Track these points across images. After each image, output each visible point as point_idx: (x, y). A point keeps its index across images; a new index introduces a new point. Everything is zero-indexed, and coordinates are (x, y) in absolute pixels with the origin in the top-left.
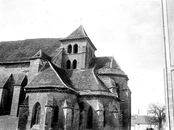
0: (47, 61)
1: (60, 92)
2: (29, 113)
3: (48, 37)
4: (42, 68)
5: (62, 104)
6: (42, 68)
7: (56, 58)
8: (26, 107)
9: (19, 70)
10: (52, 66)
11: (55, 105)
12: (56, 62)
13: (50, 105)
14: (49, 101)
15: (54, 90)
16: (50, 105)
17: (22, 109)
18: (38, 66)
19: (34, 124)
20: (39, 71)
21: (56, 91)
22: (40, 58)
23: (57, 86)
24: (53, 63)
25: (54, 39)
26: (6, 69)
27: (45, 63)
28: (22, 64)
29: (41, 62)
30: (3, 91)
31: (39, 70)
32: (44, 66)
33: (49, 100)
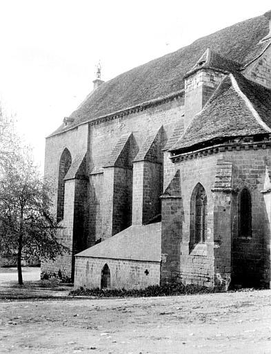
0: (225, 74)
1: (251, 147)
2: (183, 213)
3: (241, 20)
4: (213, 95)
5: (258, 183)
6: (213, 95)
7: (258, 61)
8: (175, 198)
9: (176, 113)
10: (237, 86)
11: (240, 187)
12: (258, 75)
13: (222, 189)
14: (221, 178)
15: (232, 144)
16: (222, 189)
17: (168, 204)
18: (201, 90)
19: (197, 241)
20: (203, 104)
21: (238, 148)
22: (205, 69)
23: (244, 133)
24: (246, 76)
25: (256, 19)
26: (150, 119)
27: (219, 80)
28: (179, 97)
29: (207, 79)
30: (145, 169)
31: (203, 101)
32: (217, 89)
33: (221, 175)
